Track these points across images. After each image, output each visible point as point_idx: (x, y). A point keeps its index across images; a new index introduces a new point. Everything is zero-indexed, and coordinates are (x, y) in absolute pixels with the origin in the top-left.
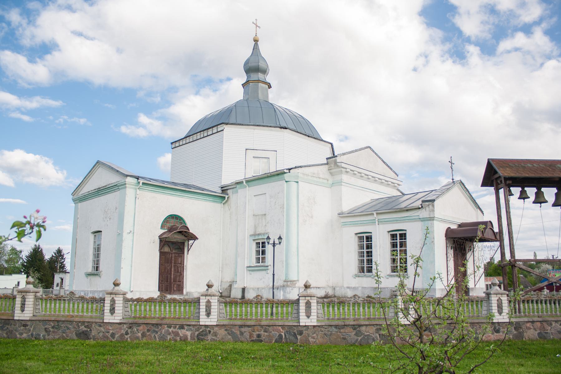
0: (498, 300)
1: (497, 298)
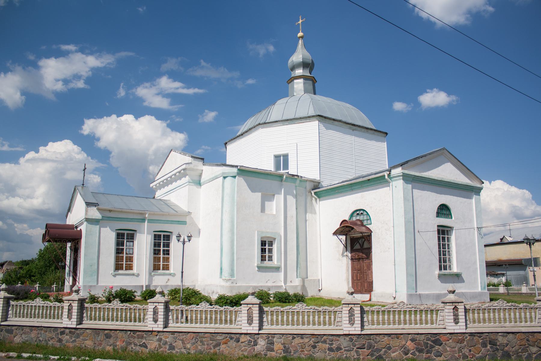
0: (453, 309)
1: (453, 307)
